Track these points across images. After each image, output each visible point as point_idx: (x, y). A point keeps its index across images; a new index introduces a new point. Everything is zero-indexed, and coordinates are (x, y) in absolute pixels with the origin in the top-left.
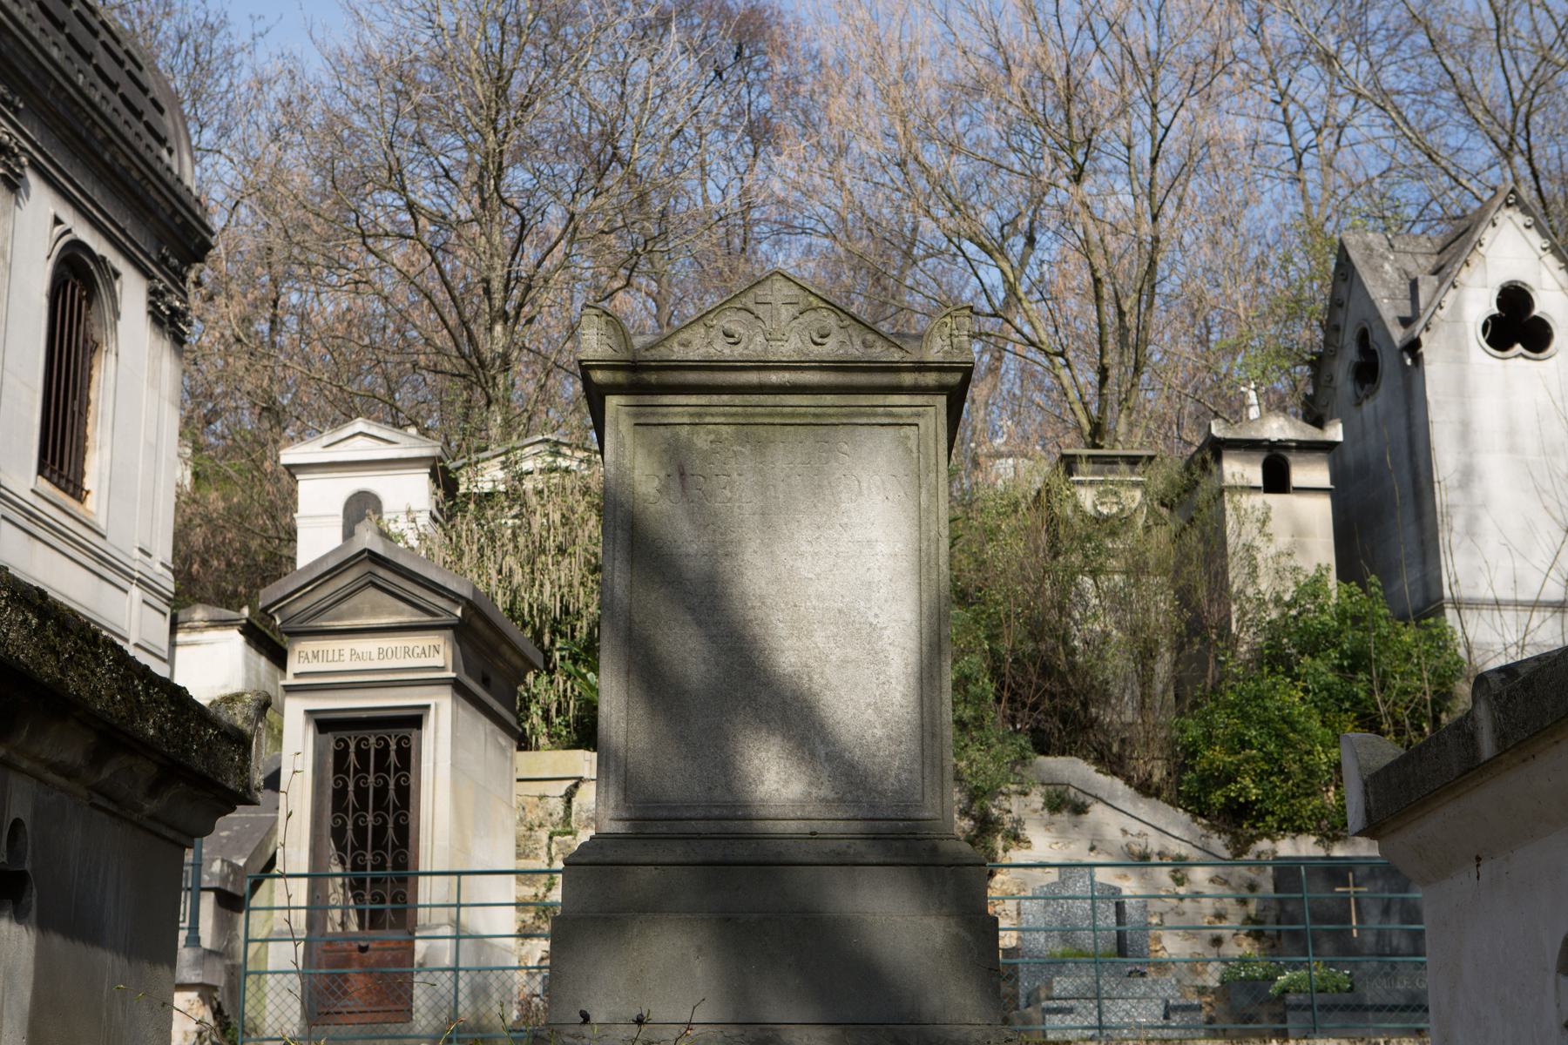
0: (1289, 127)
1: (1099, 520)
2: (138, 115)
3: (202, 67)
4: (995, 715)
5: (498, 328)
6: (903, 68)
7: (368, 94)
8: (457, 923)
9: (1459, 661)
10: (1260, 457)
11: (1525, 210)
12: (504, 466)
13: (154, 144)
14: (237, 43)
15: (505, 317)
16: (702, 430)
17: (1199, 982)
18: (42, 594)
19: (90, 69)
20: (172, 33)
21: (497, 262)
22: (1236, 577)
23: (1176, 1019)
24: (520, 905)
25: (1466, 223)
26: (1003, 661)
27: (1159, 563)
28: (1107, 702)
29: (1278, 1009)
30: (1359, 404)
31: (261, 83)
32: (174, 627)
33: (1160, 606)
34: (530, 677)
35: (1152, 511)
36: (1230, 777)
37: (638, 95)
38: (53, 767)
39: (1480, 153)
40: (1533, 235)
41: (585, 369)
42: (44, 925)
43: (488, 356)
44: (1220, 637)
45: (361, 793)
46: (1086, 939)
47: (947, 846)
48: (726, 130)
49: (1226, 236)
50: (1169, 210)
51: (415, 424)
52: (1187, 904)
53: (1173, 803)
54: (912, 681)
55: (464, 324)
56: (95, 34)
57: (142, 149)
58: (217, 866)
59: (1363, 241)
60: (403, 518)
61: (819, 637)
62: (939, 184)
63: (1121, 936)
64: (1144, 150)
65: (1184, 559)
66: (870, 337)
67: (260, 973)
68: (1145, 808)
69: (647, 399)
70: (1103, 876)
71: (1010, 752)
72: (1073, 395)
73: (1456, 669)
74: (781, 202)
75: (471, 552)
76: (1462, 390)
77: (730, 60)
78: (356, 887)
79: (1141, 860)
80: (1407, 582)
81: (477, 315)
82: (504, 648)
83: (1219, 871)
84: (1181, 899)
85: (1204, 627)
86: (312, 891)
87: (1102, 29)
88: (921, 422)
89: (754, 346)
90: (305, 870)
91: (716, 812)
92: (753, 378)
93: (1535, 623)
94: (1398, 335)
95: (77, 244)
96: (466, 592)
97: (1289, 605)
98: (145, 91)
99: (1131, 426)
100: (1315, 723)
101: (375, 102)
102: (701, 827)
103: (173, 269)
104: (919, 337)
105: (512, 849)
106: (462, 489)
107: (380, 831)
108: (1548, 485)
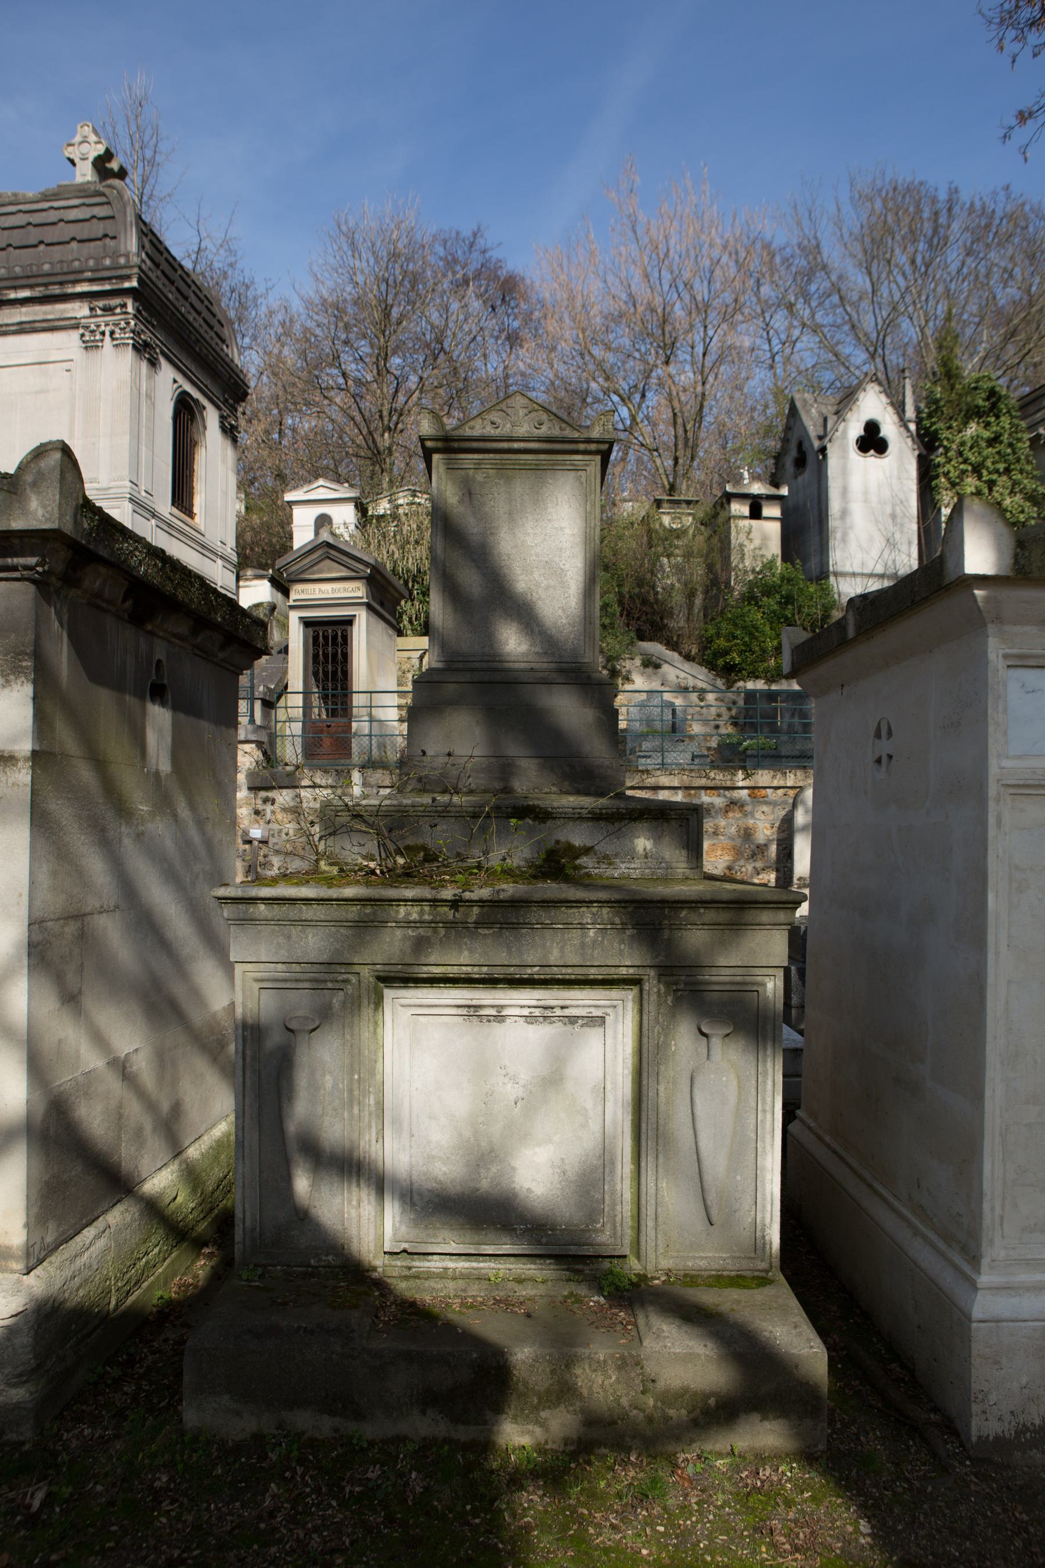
0: (769, 341)
1: (672, 530)
2: (212, 328)
3: (242, 306)
4: (620, 622)
5: (386, 435)
6: (583, 306)
7: (322, 319)
8: (370, 715)
9: (835, 601)
10: (749, 502)
11: (880, 384)
12: (390, 502)
13: (219, 342)
14: (259, 293)
15: (390, 429)
16: (480, 471)
17: (708, 745)
18: (163, 551)
19: (188, 305)
20: (228, 288)
21: (386, 402)
22: (734, 560)
23: (697, 761)
24: (399, 707)
25: (851, 390)
26: (624, 597)
27: (699, 551)
28: (672, 617)
29: (743, 757)
30: (796, 477)
31: (271, 313)
32: (238, 579)
33: (698, 572)
34: (403, 603)
35: (696, 527)
36: (726, 652)
37: (454, 317)
38: (174, 635)
39: (859, 356)
40: (883, 397)
41: (422, 440)
42: (175, 708)
43: (382, 449)
44: (726, 587)
45: (326, 656)
46: (658, 725)
47: (596, 675)
48: (497, 338)
49: (737, 394)
50: (711, 379)
51: (347, 482)
52: (704, 710)
53: (700, 664)
54: (581, 596)
55: (370, 433)
56: (189, 287)
57: (214, 345)
58: (261, 688)
59: (803, 397)
60: (342, 527)
61: (536, 575)
62: (600, 364)
63: (674, 724)
64: (699, 349)
65: (711, 550)
66: (564, 425)
67: (283, 736)
68: (687, 666)
69: (453, 456)
70: (667, 697)
71: (626, 639)
72: (661, 471)
73: (833, 605)
74: (523, 374)
75: (374, 543)
76: (844, 472)
77: (499, 302)
78: (325, 698)
79: (684, 690)
80: (813, 564)
81: (376, 429)
82: (390, 588)
83: (720, 695)
84: (702, 707)
85: (718, 583)
86: (305, 700)
87: (681, 287)
88: (588, 469)
89: (505, 430)
90: (301, 690)
91: (486, 658)
92: (505, 445)
93: (870, 583)
94: (816, 444)
95: (185, 393)
96: (372, 561)
97: (758, 573)
98: (214, 315)
99: (688, 487)
100: (767, 629)
101: (326, 321)
102: (478, 665)
103: (231, 406)
104: (588, 427)
105: (395, 682)
106: (370, 513)
107: (334, 673)
108: (880, 519)
